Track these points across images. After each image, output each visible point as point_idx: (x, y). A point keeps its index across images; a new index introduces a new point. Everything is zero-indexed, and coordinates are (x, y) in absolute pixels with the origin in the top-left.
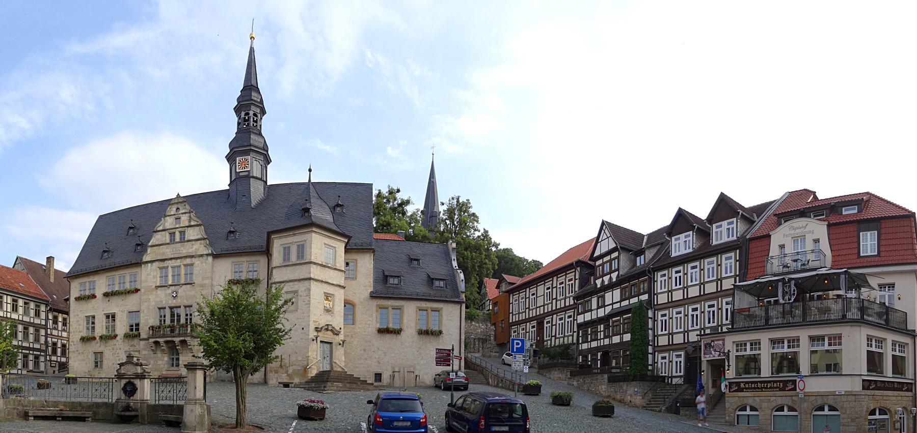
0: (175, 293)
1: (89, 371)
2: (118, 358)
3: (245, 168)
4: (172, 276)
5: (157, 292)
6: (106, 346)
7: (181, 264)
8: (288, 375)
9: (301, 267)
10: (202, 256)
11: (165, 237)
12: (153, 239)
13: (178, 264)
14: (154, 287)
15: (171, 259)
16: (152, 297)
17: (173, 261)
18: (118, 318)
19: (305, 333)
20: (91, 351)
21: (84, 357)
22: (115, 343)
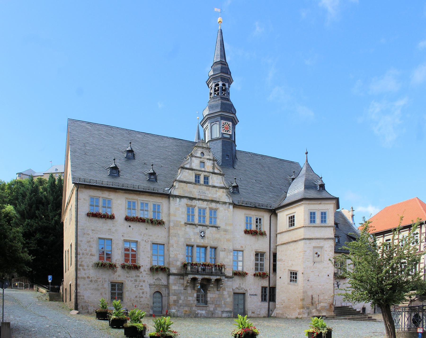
0: (203, 233)
5: (185, 229)
6: (127, 277)
8: (317, 310)
9: (325, 229)
10: (225, 203)
11: (189, 176)
15: (199, 199)
16: (181, 233)
17: (200, 202)
18: (141, 247)
19: (330, 279)
20: (107, 280)
22: (139, 275)
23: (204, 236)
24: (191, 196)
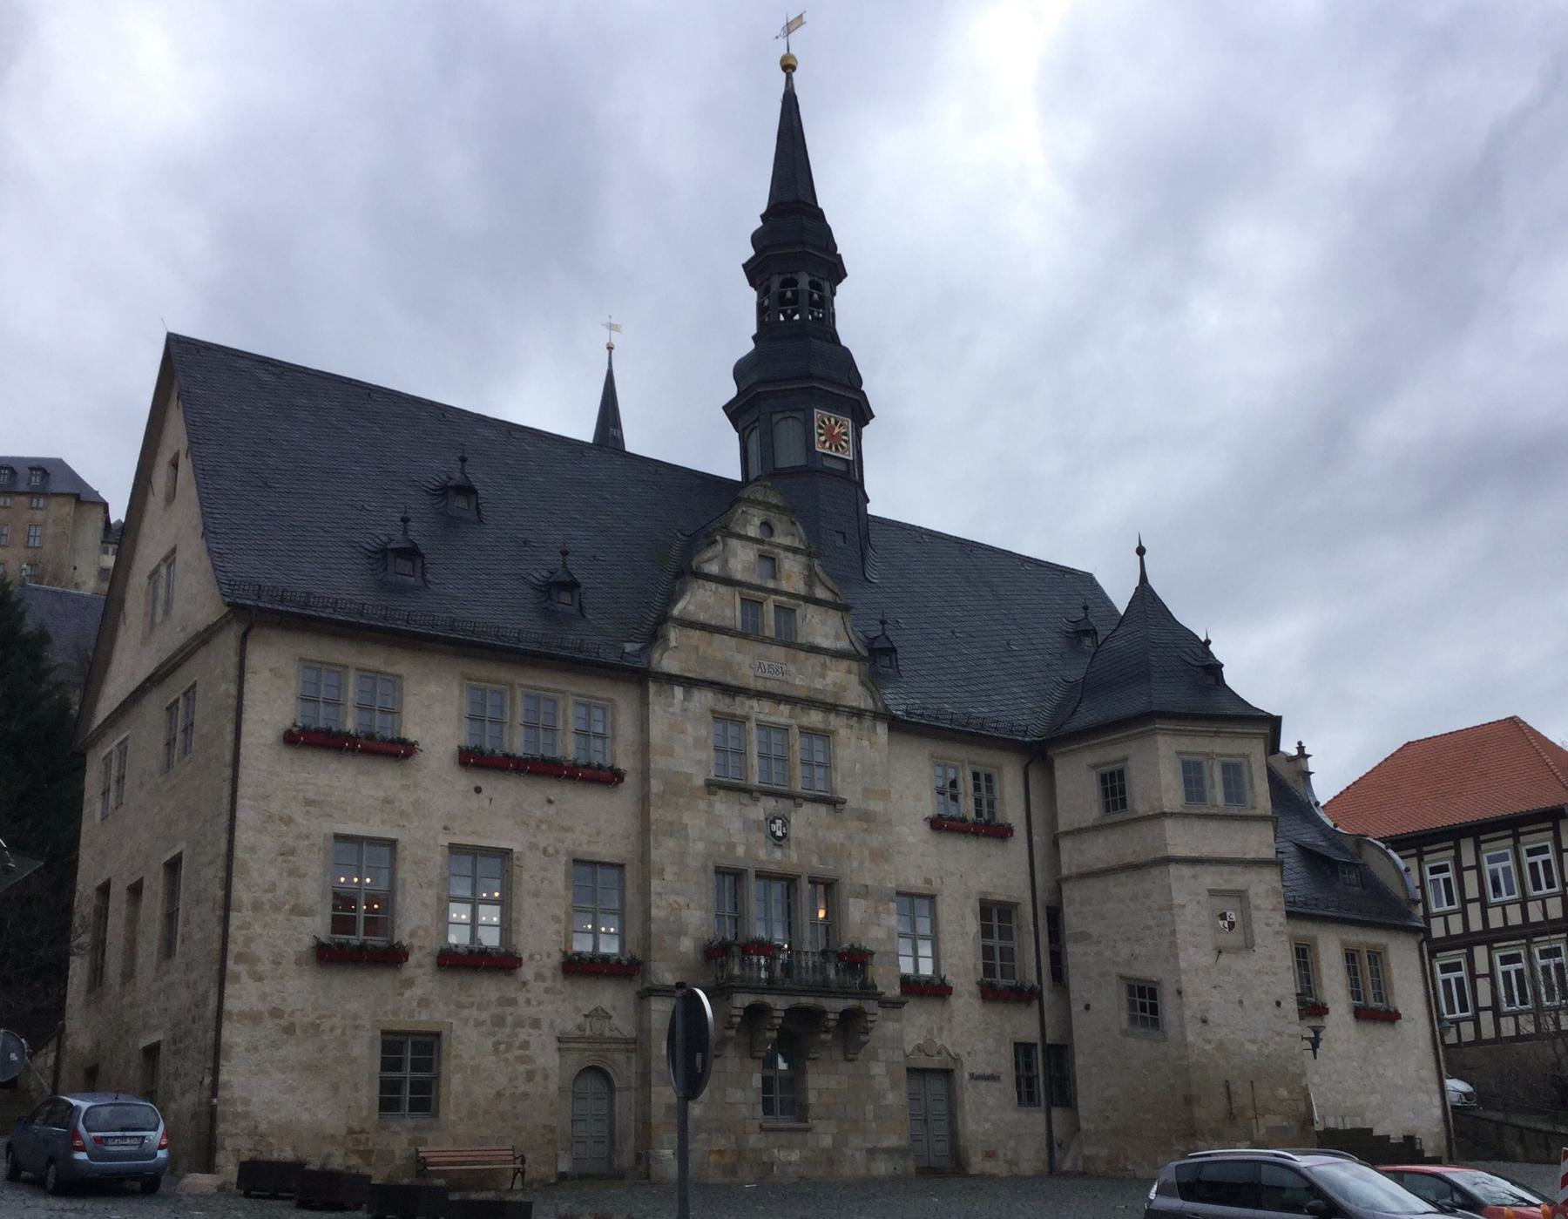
0: (779, 822)
1: (351, 1131)
2: (522, 1068)
3: (837, 449)
4: (760, 756)
5: (711, 805)
6: (461, 1006)
7: (792, 721)
12: (687, 597)
13: (783, 721)
14: (699, 781)
16: (694, 821)
18: (526, 876)
21: (322, 1049)
23: (785, 835)
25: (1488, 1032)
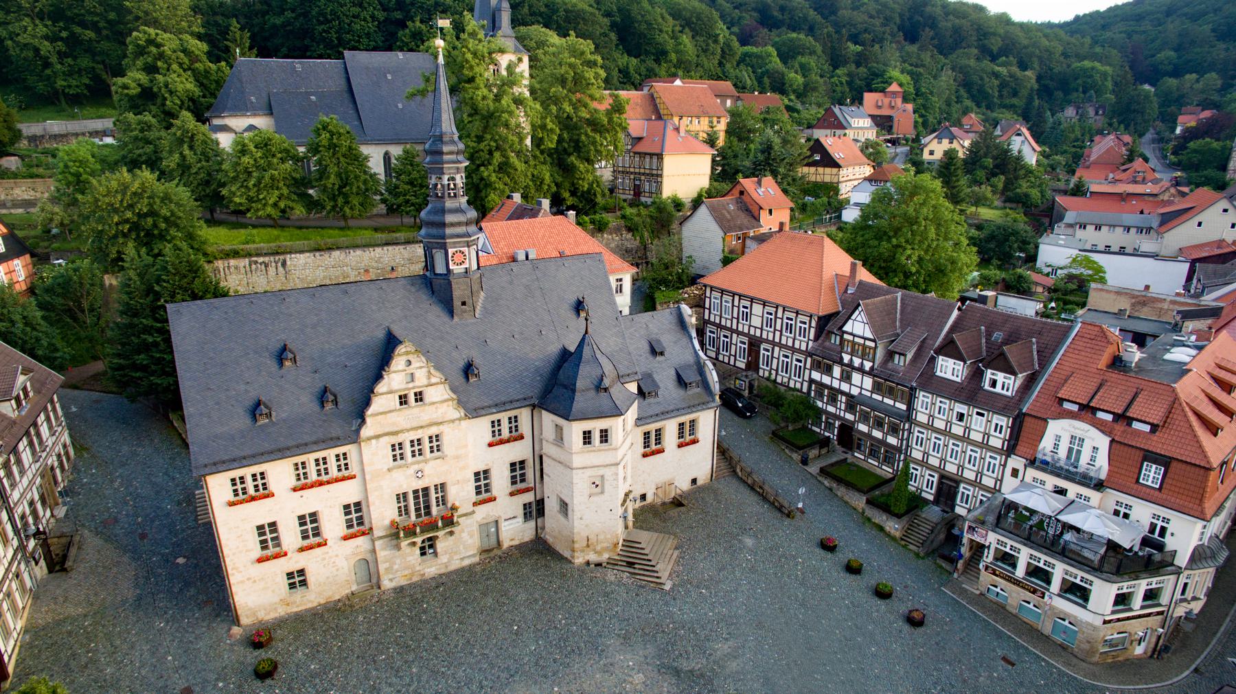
10: (453, 421)
24: (396, 429)
25: (773, 377)
